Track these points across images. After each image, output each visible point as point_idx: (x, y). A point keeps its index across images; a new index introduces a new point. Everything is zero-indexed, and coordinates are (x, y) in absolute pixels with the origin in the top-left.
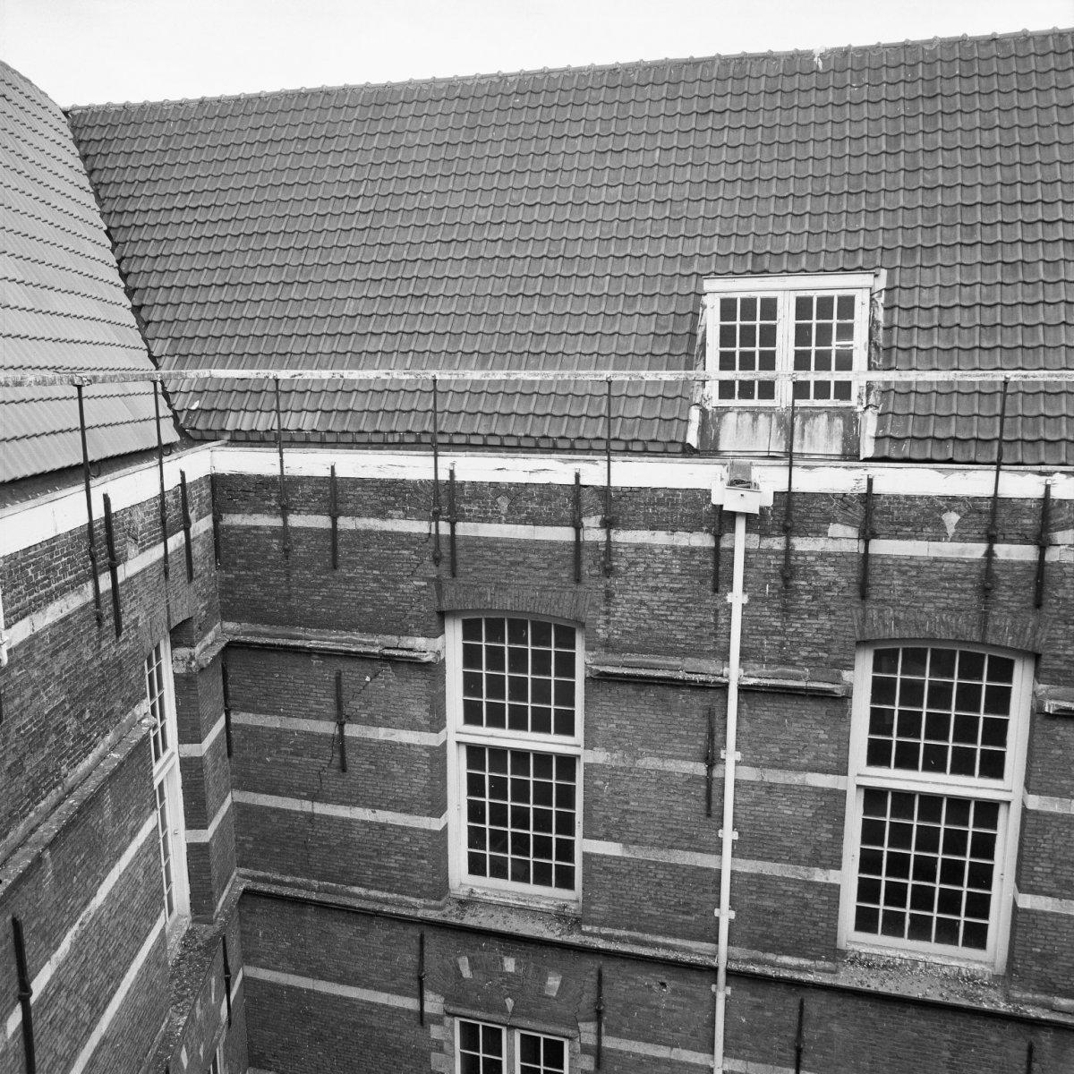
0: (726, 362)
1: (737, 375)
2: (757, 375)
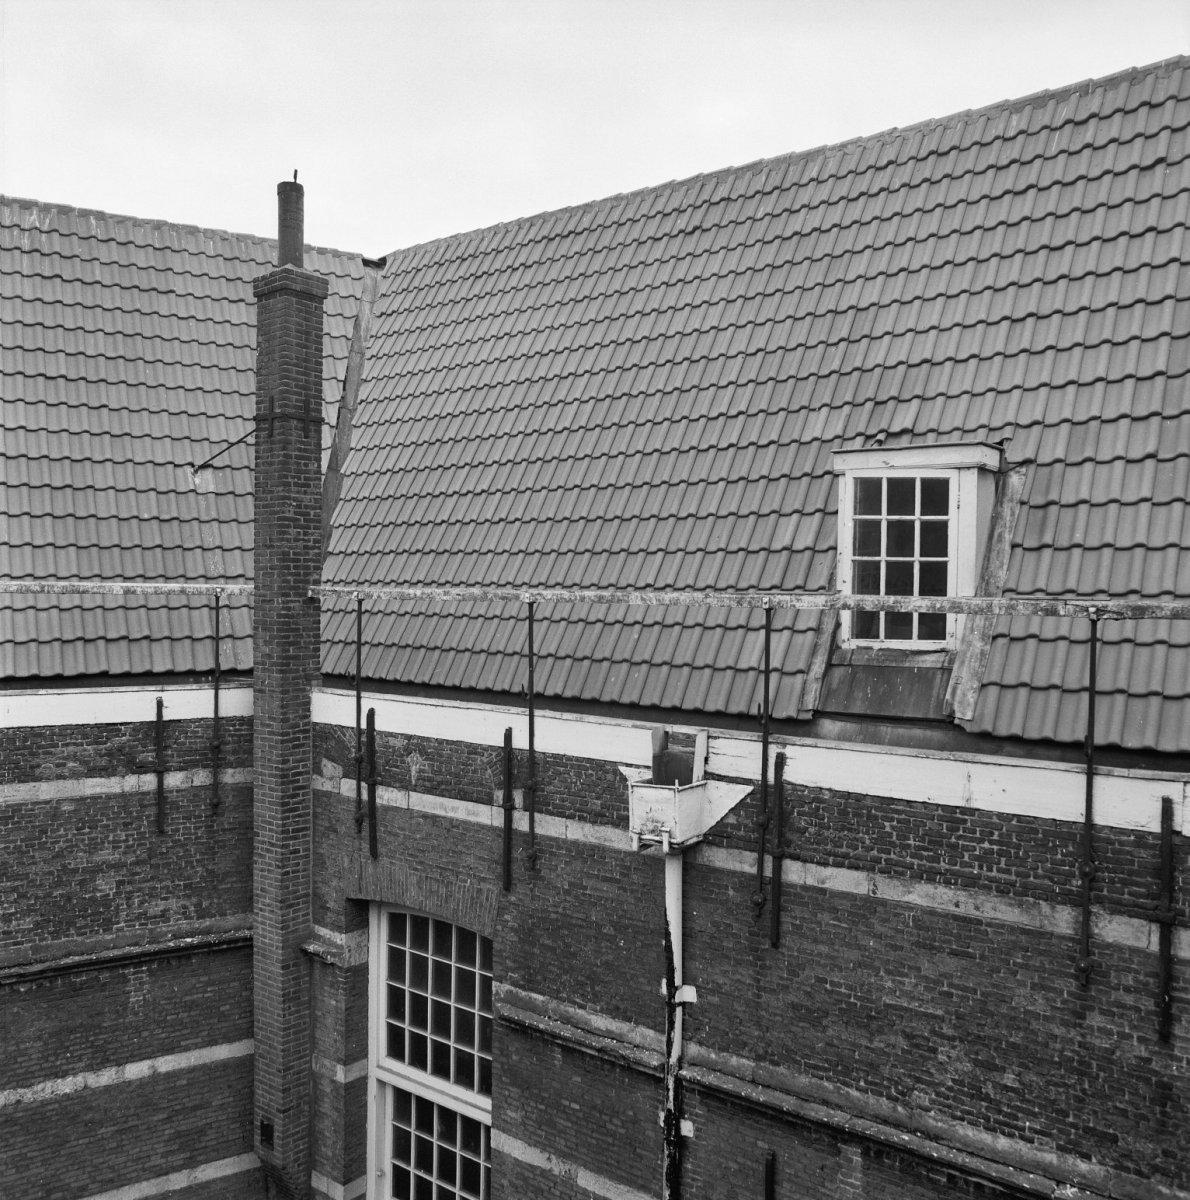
0: (866, 579)
1: (880, 600)
2: (916, 603)
